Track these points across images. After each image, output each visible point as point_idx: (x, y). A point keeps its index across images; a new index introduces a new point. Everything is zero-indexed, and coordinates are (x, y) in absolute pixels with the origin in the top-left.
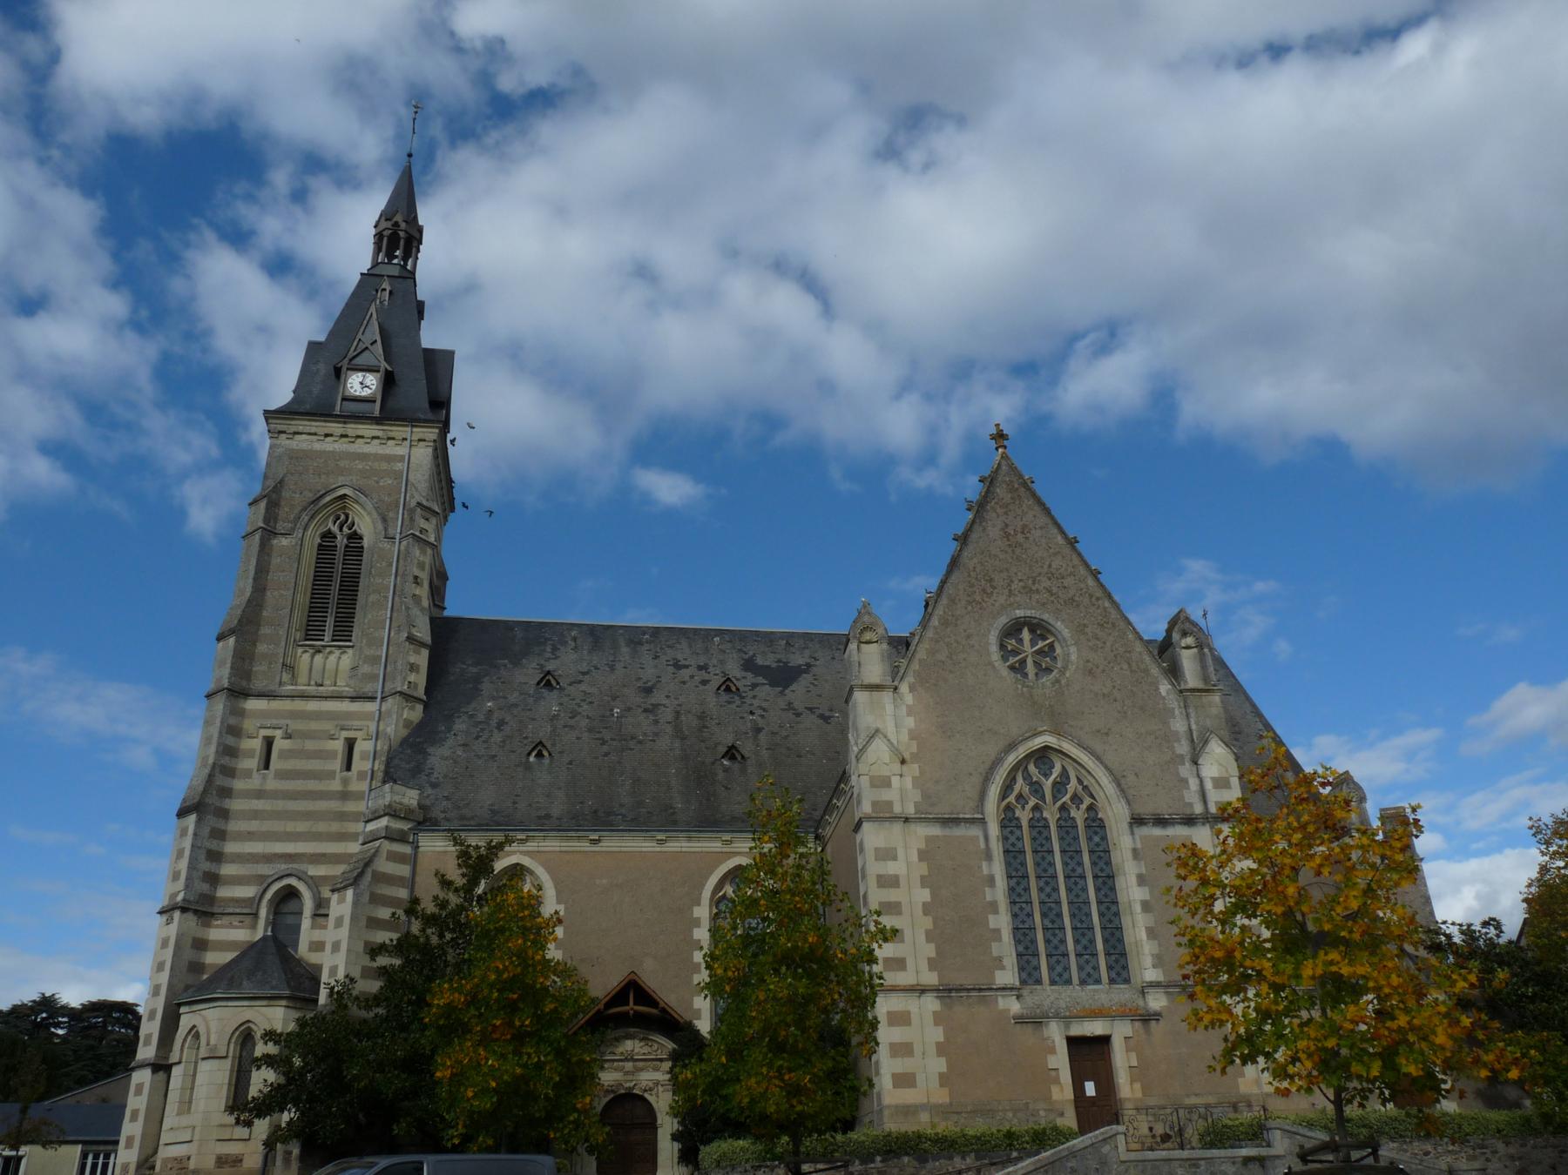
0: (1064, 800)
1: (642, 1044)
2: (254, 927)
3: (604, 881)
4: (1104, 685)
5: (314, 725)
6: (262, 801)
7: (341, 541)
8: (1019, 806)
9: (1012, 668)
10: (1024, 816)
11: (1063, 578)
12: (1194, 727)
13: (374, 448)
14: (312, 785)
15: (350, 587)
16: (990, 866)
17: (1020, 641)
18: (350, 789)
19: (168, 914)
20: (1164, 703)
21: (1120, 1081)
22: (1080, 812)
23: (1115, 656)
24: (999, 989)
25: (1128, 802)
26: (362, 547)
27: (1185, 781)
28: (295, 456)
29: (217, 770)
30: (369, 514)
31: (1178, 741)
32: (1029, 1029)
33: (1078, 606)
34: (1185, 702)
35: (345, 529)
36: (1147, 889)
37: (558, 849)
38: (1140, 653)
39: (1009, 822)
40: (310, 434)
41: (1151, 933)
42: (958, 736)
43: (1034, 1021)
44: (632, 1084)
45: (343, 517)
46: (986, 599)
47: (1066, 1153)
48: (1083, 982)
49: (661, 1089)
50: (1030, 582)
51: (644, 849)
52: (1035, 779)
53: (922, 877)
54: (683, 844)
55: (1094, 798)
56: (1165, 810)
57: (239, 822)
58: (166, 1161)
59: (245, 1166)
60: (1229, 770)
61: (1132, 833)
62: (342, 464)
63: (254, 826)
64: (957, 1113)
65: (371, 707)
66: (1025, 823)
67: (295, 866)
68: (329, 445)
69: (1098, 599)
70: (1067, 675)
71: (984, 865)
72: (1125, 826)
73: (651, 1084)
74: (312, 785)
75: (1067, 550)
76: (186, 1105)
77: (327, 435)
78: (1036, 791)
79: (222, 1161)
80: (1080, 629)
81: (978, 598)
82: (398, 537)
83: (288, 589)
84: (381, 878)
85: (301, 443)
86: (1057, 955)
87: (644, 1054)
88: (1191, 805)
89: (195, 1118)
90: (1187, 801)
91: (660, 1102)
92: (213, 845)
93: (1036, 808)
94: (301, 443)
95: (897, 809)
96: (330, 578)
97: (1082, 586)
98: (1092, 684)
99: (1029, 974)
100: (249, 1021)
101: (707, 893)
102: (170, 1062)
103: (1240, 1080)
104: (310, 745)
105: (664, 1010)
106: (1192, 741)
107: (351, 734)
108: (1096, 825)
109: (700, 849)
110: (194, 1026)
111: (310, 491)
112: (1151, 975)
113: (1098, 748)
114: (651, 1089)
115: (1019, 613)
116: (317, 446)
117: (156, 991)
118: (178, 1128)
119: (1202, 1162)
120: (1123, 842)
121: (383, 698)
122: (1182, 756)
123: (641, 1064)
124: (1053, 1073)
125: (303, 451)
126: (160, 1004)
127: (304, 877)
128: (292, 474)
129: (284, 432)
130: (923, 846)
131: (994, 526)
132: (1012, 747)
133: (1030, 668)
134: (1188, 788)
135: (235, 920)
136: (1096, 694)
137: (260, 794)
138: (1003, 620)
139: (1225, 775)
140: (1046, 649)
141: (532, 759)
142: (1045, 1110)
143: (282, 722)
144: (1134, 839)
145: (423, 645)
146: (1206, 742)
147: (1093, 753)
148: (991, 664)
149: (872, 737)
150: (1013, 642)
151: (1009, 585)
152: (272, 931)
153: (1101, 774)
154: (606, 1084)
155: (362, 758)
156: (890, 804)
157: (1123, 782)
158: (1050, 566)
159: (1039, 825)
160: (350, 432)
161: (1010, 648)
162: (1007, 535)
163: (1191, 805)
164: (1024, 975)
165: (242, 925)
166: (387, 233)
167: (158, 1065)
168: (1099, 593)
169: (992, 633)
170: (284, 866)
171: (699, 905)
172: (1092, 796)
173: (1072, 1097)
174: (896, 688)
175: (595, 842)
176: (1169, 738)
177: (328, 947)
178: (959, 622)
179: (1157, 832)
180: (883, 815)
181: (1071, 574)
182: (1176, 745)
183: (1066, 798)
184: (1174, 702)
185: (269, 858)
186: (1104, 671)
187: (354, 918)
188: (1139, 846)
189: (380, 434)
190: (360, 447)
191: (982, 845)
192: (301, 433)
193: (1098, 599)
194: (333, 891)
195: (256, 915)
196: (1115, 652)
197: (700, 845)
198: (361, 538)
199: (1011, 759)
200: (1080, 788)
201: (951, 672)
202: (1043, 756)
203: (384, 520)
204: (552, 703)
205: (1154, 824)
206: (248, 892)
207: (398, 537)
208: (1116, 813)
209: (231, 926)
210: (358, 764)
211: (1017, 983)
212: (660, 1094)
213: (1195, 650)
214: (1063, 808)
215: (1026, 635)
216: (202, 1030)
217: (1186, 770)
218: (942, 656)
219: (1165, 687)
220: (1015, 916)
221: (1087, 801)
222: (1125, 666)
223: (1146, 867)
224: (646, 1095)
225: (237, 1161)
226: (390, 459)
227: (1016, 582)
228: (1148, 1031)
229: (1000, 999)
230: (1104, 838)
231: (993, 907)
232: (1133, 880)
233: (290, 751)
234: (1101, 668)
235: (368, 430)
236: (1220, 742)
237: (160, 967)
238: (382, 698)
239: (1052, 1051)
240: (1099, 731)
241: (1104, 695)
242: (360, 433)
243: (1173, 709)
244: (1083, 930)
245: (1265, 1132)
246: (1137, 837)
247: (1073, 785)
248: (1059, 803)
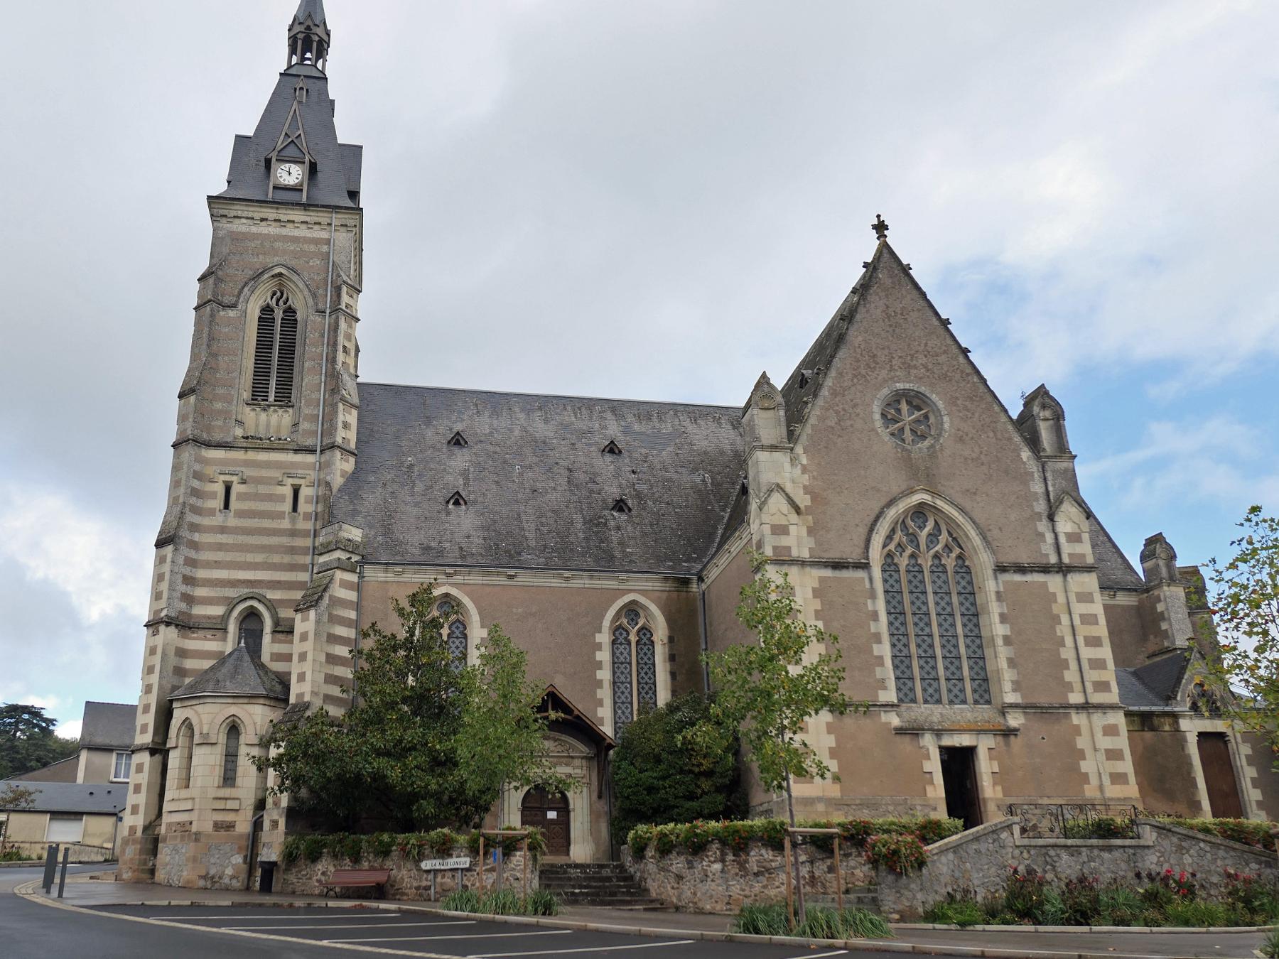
0: (936, 549)
2: (224, 639)
4: (973, 451)
5: (265, 473)
6: (225, 536)
7: (279, 315)
8: (898, 553)
9: (892, 434)
10: (903, 562)
11: (937, 356)
12: (1051, 489)
13: (302, 232)
14: (267, 524)
15: (288, 352)
16: (874, 603)
17: (899, 411)
18: (297, 527)
19: (154, 627)
20: (1025, 468)
21: (985, 784)
22: (949, 560)
23: (982, 426)
24: (883, 705)
25: (994, 552)
26: (296, 320)
27: (1043, 535)
28: (236, 238)
29: (187, 509)
30: (301, 291)
31: (1037, 500)
32: (907, 739)
33: (950, 380)
34: (1043, 467)
35: (281, 302)
36: (1008, 626)
37: (480, 582)
38: (1005, 423)
39: (889, 564)
40: (247, 218)
41: (1012, 663)
42: (846, 492)
43: (912, 731)
45: (279, 294)
46: (870, 373)
47: (971, 837)
48: (951, 702)
50: (909, 358)
51: (552, 585)
52: (911, 531)
53: (816, 611)
54: (586, 582)
55: (962, 549)
56: (1025, 559)
57: (207, 553)
58: (169, 825)
59: (237, 830)
60: (1081, 527)
61: (996, 578)
62: (276, 245)
63: (219, 556)
64: (847, 805)
65: (310, 458)
66: (902, 568)
67: (255, 590)
68: (263, 229)
69: (968, 375)
70: (941, 441)
71: (869, 601)
72: (990, 572)
74: (267, 524)
75: (941, 331)
76: (186, 783)
77: (262, 220)
78: (912, 541)
79: (218, 826)
80: (952, 402)
81: (863, 372)
82: (328, 311)
83: (237, 355)
84: (336, 602)
85: (241, 226)
86: (930, 678)
87: (558, 752)
88: (1047, 555)
89: (193, 791)
90: (1044, 552)
92: (188, 571)
93: (913, 556)
94: (241, 226)
95: (795, 553)
96: (270, 347)
97: (955, 363)
98: (962, 450)
99: (906, 695)
100: (233, 715)
101: (606, 623)
102: (168, 746)
103: (1086, 786)
104: (263, 489)
105: (578, 717)
106: (1049, 500)
107: (297, 481)
108: (964, 569)
109: (600, 586)
110: (187, 718)
111: (250, 269)
112: (1011, 698)
113: (967, 505)
115: (900, 386)
116: (254, 229)
117: (148, 689)
118: (179, 800)
119: (1084, 849)
120: (990, 585)
121: (322, 451)
122: (1039, 514)
124: (928, 776)
125: (243, 233)
126: (153, 700)
127: (263, 600)
128: (234, 254)
129: (225, 216)
130: (816, 585)
131: (876, 307)
132: (891, 503)
133: (908, 434)
134: (1045, 542)
135: (209, 634)
136: (966, 459)
137: (223, 530)
138: (885, 391)
139: (1078, 531)
140: (922, 418)
141: (451, 506)
142: (921, 805)
143: (238, 469)
144: (997, 583)
145: (353, 406)
146: (1061, 502)
147: (962, 510)
148: (873, 430)
149: (770, 491)
150: (892, 411)
151: (891, 361)
152: (245, 643)
153: (969, 528)
155: (306, 502)
156: (789, 548)
157: (988, 534)
158: (926, 345)
159: (915, 570)
160: (283, 218)
161: (889, 417)
162: (889, 317)
163: (1047, 555)
164: (901, 695)
165: (214, 637)
166: (301, 36)
167: (155, 749)
168: (969, 370)
169: (876, 403)
170: (246, 591)
171: (600, 632)
172: (960, 547)
173: (944, 795)
174: (792, 449)
175: (511, 577)
176: (1029, 498)
177: (295, 658)
178: (846, 393)
179: (1018, 578)
180: (783, 560)
181: (945, 352)
182: (1035, 504)
183: (939, 548)
184: (1033, 467)
185: (233, 584)
186: (972, 438)
187: (317, 634)
188: (1002, 589)
189: (307, 219)
190: (289, 231)
191: (867, 585)
192: (240, 218)
193: (968, 375)
194: (296, 611)
195: (225, 630)
196: (982, 422)
197: (600, 582)
198: (295, 312)
199: (892, 513)
200: (950, 539)
201: (839, 436)
202: (920, 512)
203: (314, 296)
204: (461, 460)
205: (1015, 572)
206: (218, 611)
207: (328, 311)
208: (983, 561)
209: (205, 638)
210: (303, 507)
211: (896, 701)
213: (1051, 422)
214: (937, 556)
215: (904, 407)
216: (195, 722)
217: (1043, 526)
218: (832, 422)
219: (1026, 454)
220: (893, 645)
221: (957, 551)
222: (991, 435)
223: (1008, 608)
225: (230, 826)
226: (317, 241)
227: (897, 358)
228: (1007, 744)
229: (882, 713)
230: (970, 583)
231: (877, 638)
232: (996, 618)
233: (245, 494)
234: (970, 436)
235: (297, 215)
236: (1073, 502)
237: (149, 670)
238: (321, 451)
239: (928, 757)
240: (968, 491)
241: (972, 459)
242: (291, 218)
243: (1033, 472)
244: (953, 660)
245: (1135, 827)
246: (1000, 581)
247: (944, 537)
248: (932, 552)
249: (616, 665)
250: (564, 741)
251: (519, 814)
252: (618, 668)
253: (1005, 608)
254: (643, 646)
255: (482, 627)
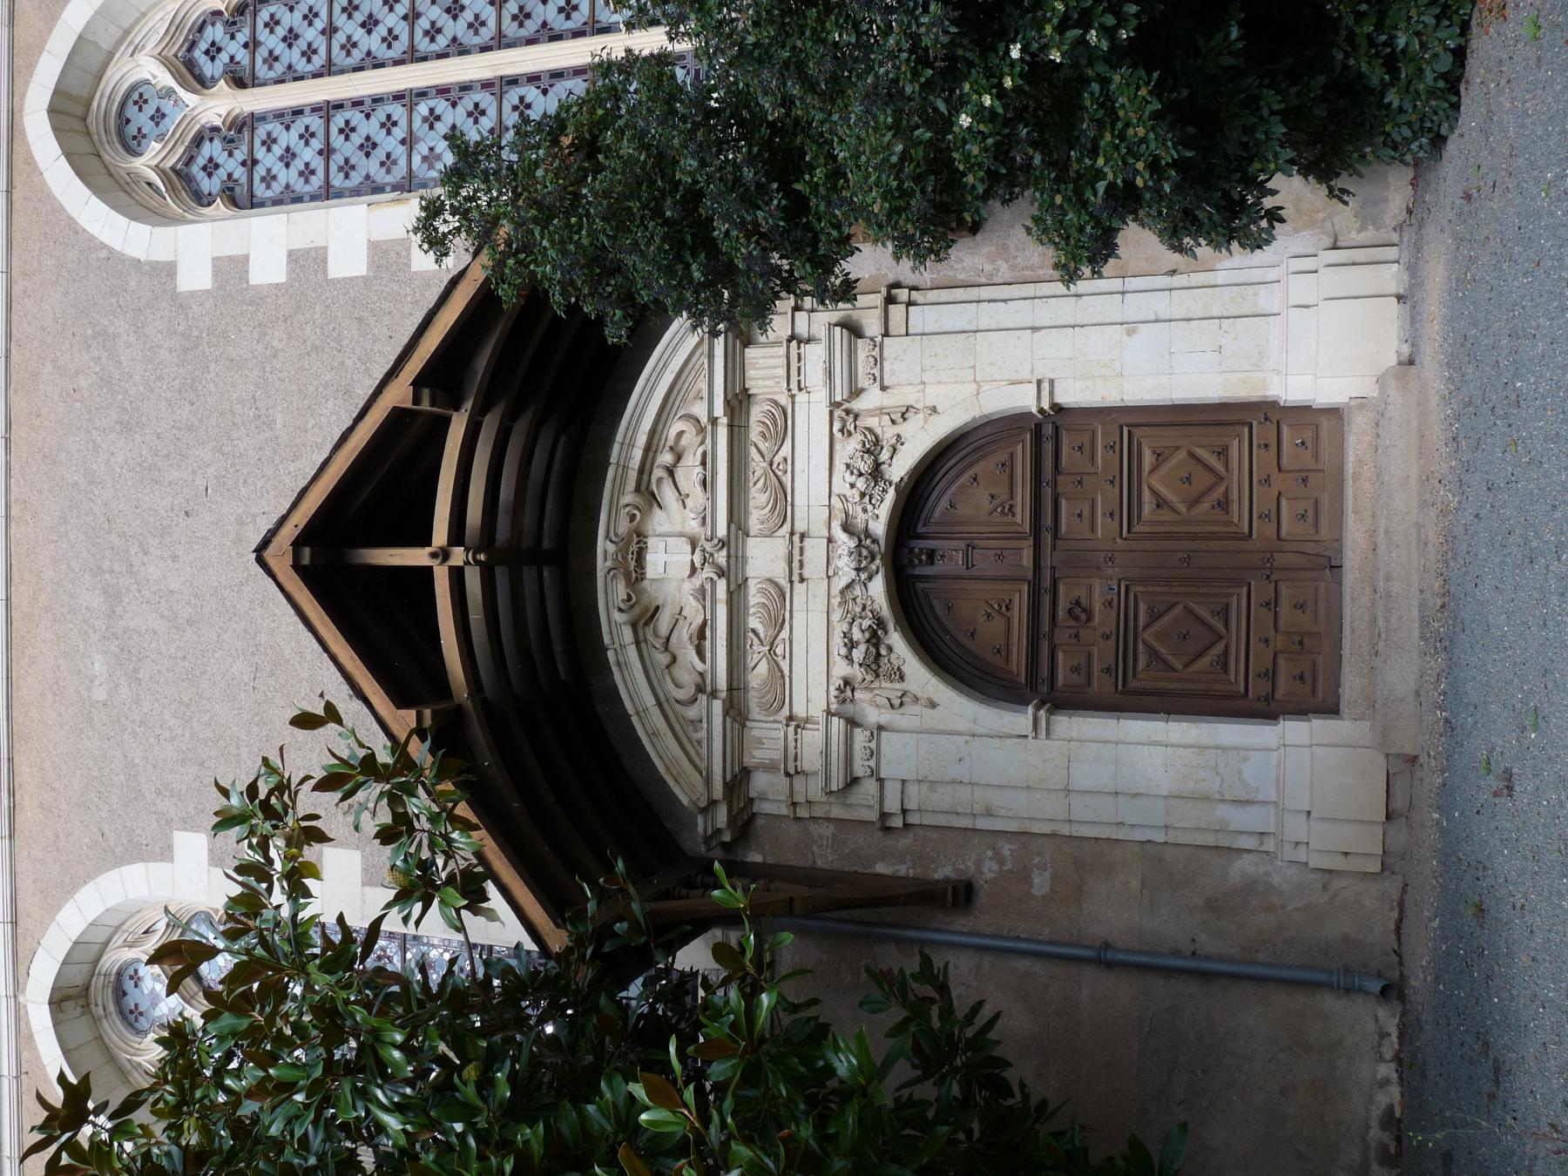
1: (668, 494)
3: (99, 666)
44: (845, 542)
49: (871, 399)
73: (849, 448)
91: (932, 396)
114: (872, 447)
123: (758, 500)
154: (841, 669)
212: (891, 400)
224: (899, 468)
249: (337, 181)
250: (650, 449)
251: (1072, 726)
252: (347, 168)
253: (884, 510)
254: (262, 53)
255: (165, 853)
